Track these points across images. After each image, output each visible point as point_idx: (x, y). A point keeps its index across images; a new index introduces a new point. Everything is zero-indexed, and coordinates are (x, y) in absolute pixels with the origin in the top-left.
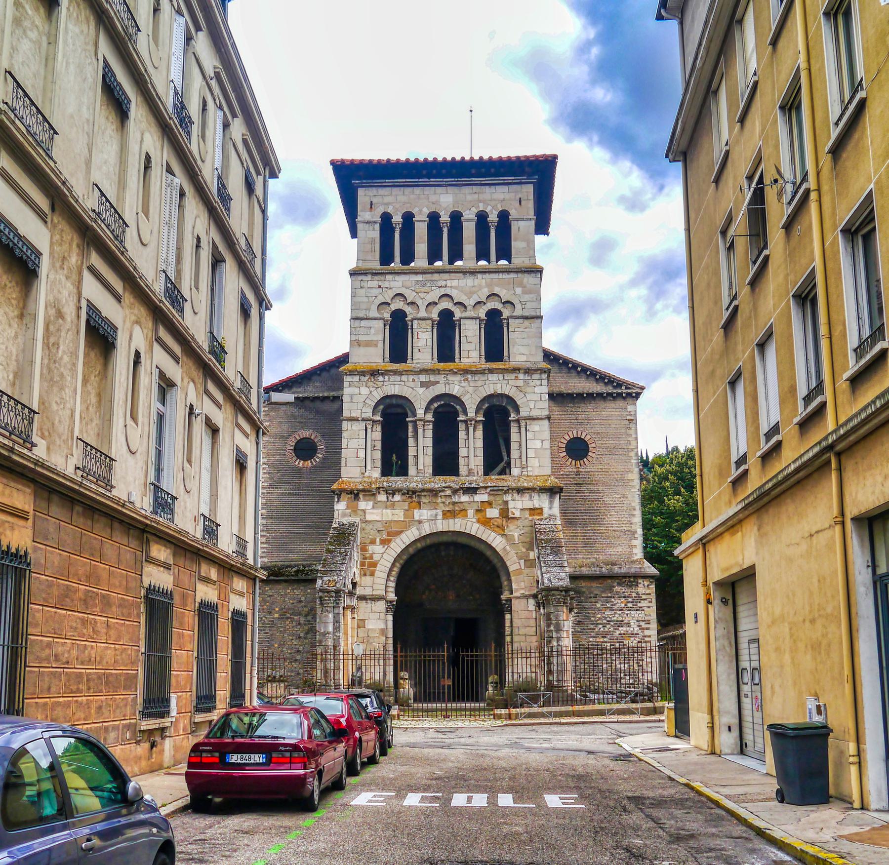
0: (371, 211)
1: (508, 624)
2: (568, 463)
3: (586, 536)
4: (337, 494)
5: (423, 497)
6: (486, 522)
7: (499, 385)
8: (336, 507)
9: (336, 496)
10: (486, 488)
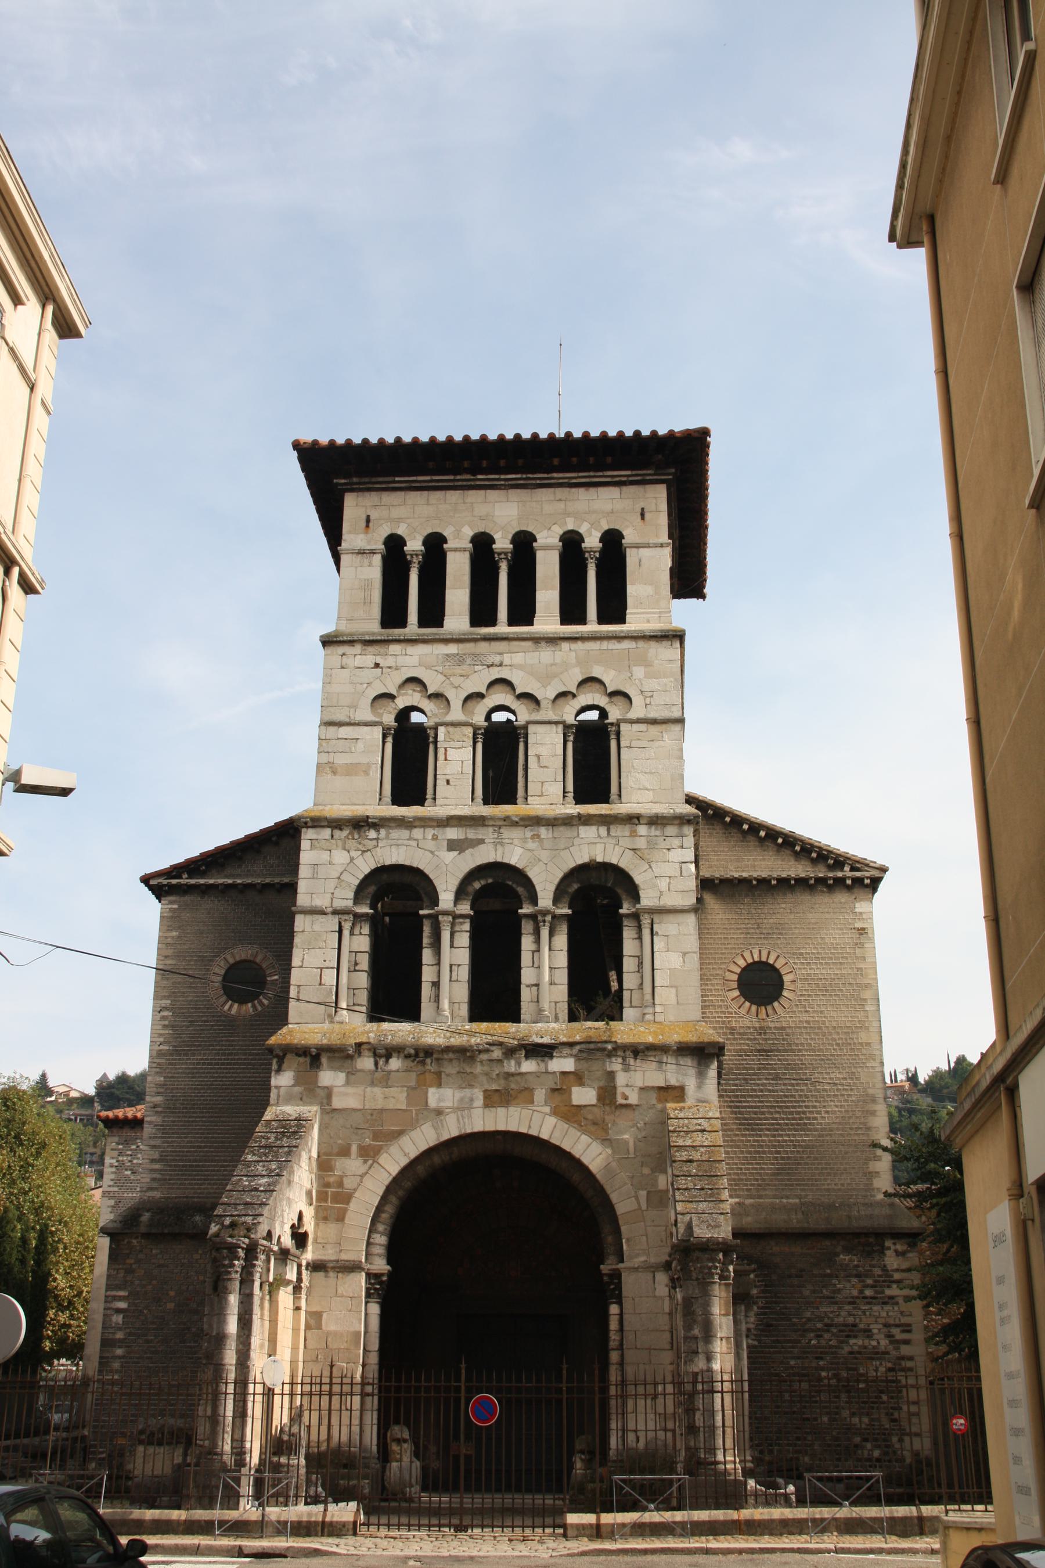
0: (366, 533)
1: (613, 1325)
2: (743, 1011)
3: (778, 1152)
4: (277, 1056)
5: (446, 1063)
6: (571, 1114)
7: (599, 848)
8: (273, 1082)
9: (275, 1061)
10: (571, 1045)
